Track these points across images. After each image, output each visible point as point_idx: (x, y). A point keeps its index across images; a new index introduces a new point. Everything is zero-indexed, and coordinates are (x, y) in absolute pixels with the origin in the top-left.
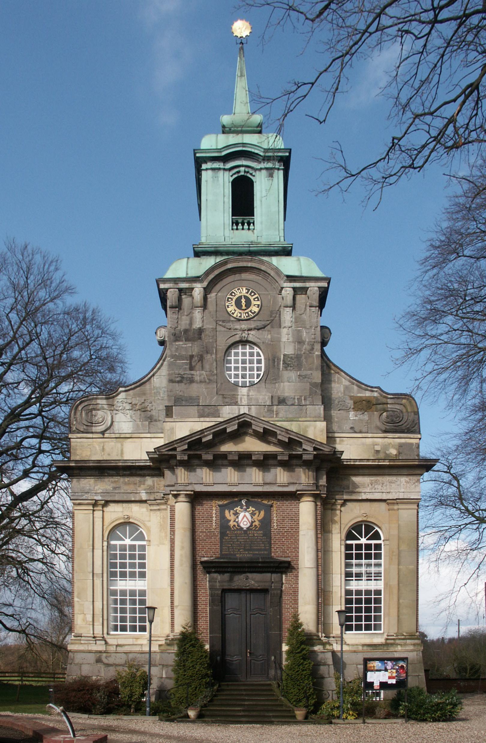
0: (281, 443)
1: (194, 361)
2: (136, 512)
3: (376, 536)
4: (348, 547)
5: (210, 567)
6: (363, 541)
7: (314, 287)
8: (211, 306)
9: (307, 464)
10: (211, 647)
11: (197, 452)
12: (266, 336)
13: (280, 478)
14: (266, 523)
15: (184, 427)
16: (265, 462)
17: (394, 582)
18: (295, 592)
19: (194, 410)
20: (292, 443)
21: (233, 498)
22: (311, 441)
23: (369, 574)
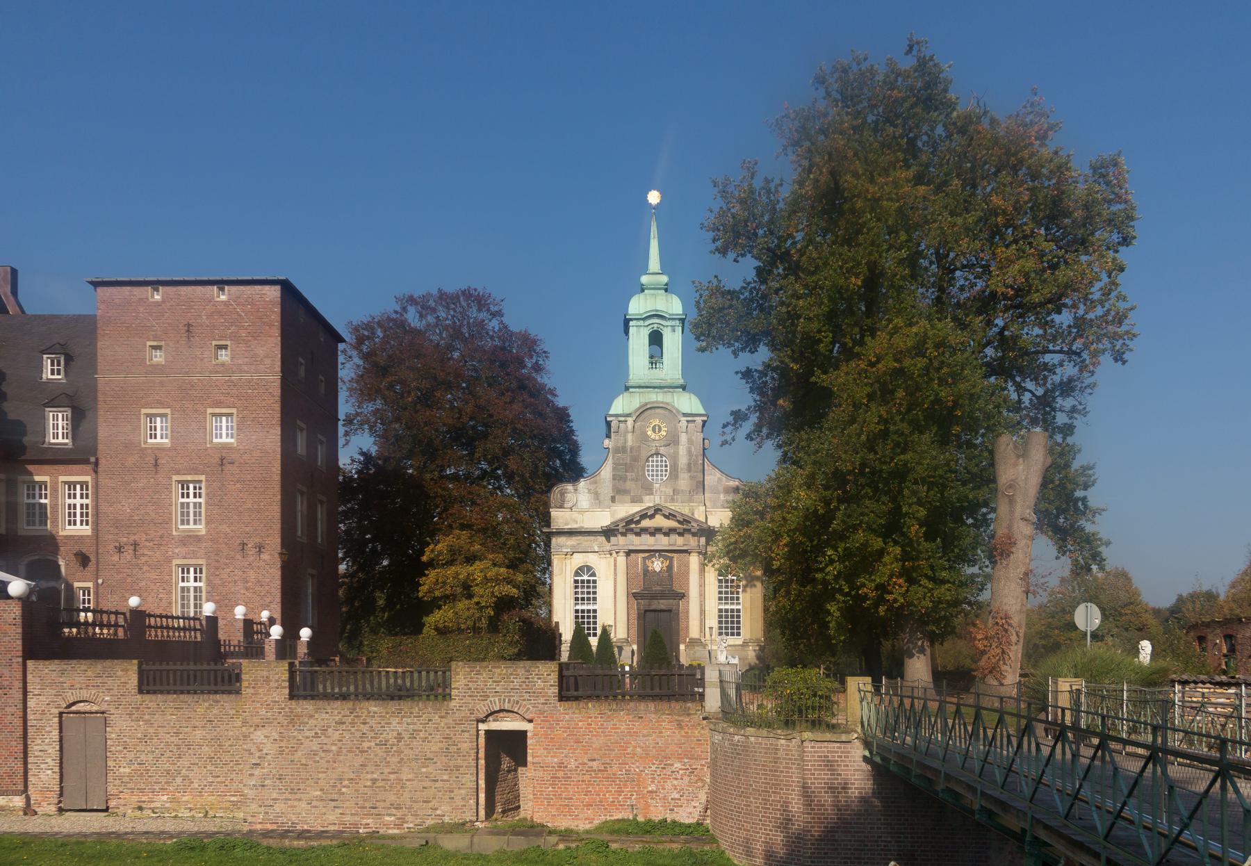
0: (679, 522)
1: (628, 468)
2: (591, 560)
3: (594, 575)
4: (576, 582)
5: (635, 596)
6: (585, 578)
7: (699, 420)
8: (638, 432)
9: (694, 535)
10: (70, 639)
11: (629, 526)
12: (671, 450)
13: (678, 542)
14: (670, 568)
15: (626, 509)
16: (668, 532)
17: (748, 605)
18: (687, 612)
19: (628, 498)
20: (685, 521)
21: (652, 552)
22: (696, 521)
23: (589, 599)
